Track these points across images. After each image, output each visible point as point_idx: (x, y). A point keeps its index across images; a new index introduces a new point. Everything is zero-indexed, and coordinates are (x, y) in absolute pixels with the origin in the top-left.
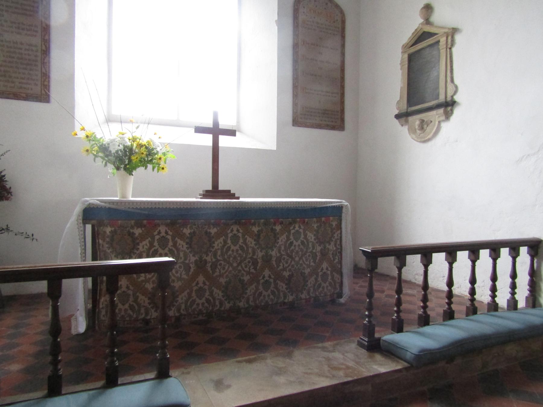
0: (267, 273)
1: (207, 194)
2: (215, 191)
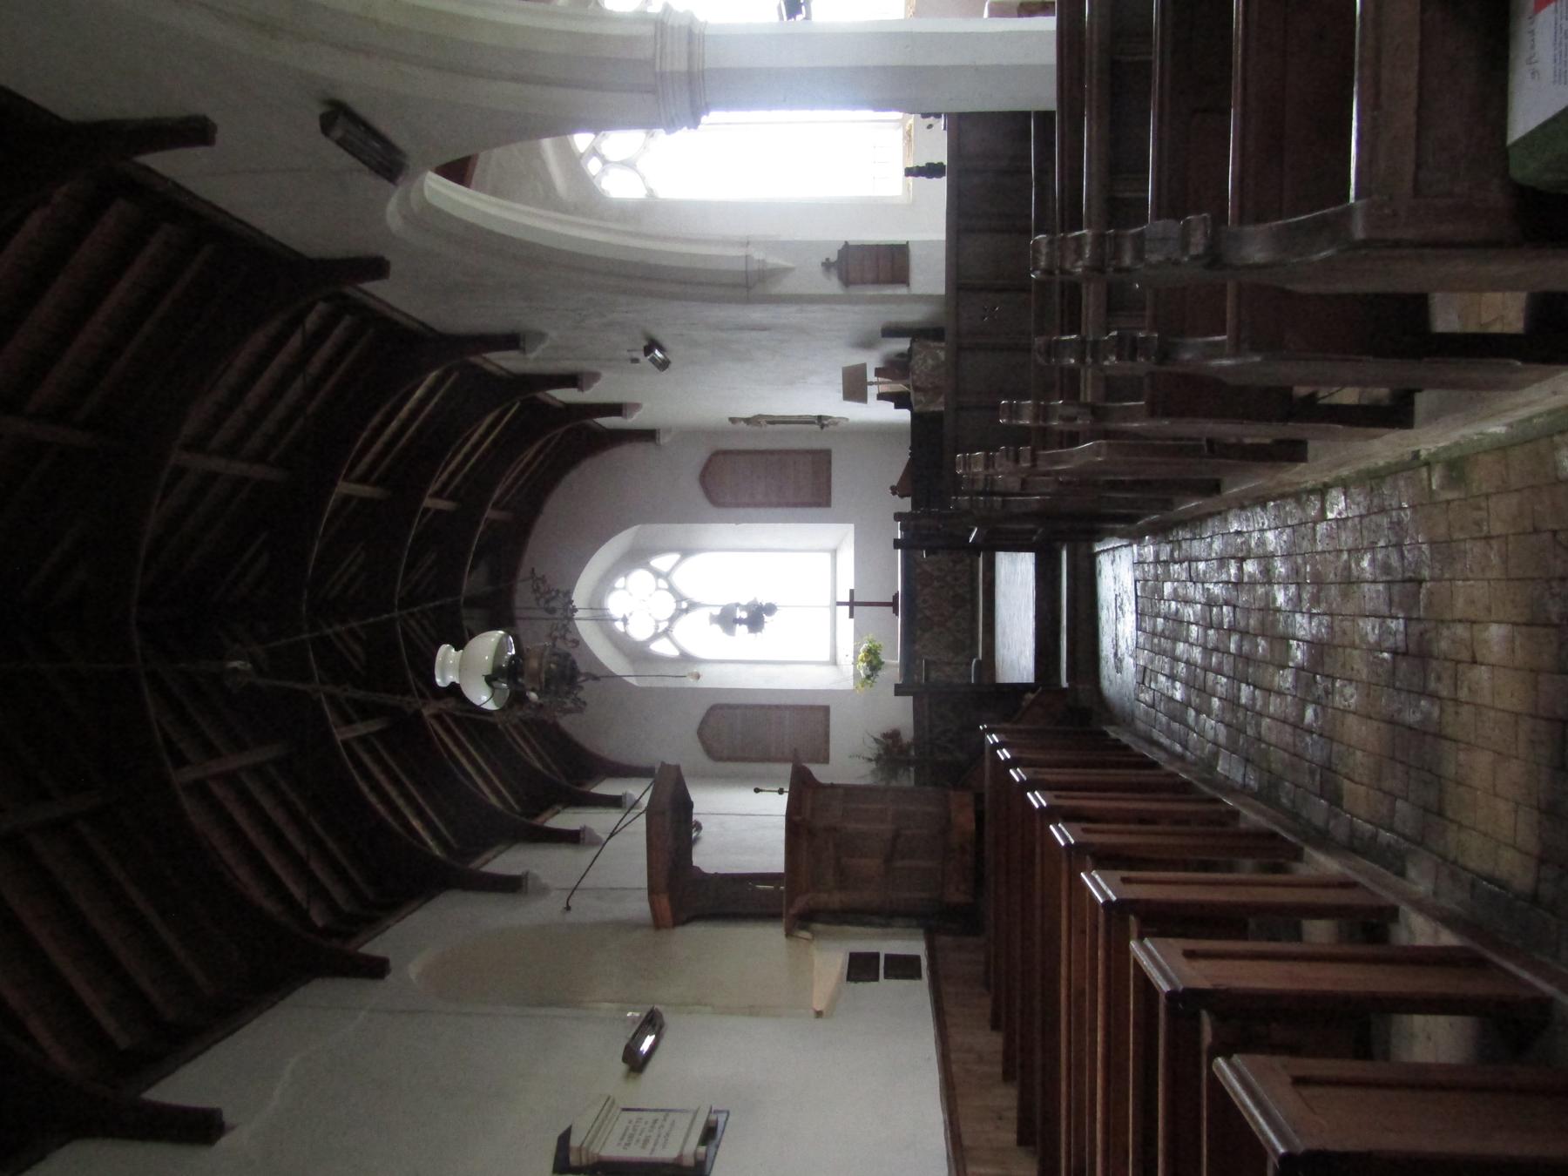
0: (949, 578)
1: (895, 611)
2: (894, 604)
